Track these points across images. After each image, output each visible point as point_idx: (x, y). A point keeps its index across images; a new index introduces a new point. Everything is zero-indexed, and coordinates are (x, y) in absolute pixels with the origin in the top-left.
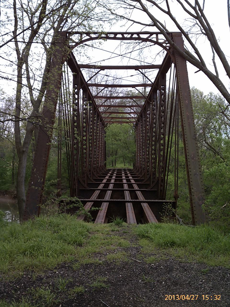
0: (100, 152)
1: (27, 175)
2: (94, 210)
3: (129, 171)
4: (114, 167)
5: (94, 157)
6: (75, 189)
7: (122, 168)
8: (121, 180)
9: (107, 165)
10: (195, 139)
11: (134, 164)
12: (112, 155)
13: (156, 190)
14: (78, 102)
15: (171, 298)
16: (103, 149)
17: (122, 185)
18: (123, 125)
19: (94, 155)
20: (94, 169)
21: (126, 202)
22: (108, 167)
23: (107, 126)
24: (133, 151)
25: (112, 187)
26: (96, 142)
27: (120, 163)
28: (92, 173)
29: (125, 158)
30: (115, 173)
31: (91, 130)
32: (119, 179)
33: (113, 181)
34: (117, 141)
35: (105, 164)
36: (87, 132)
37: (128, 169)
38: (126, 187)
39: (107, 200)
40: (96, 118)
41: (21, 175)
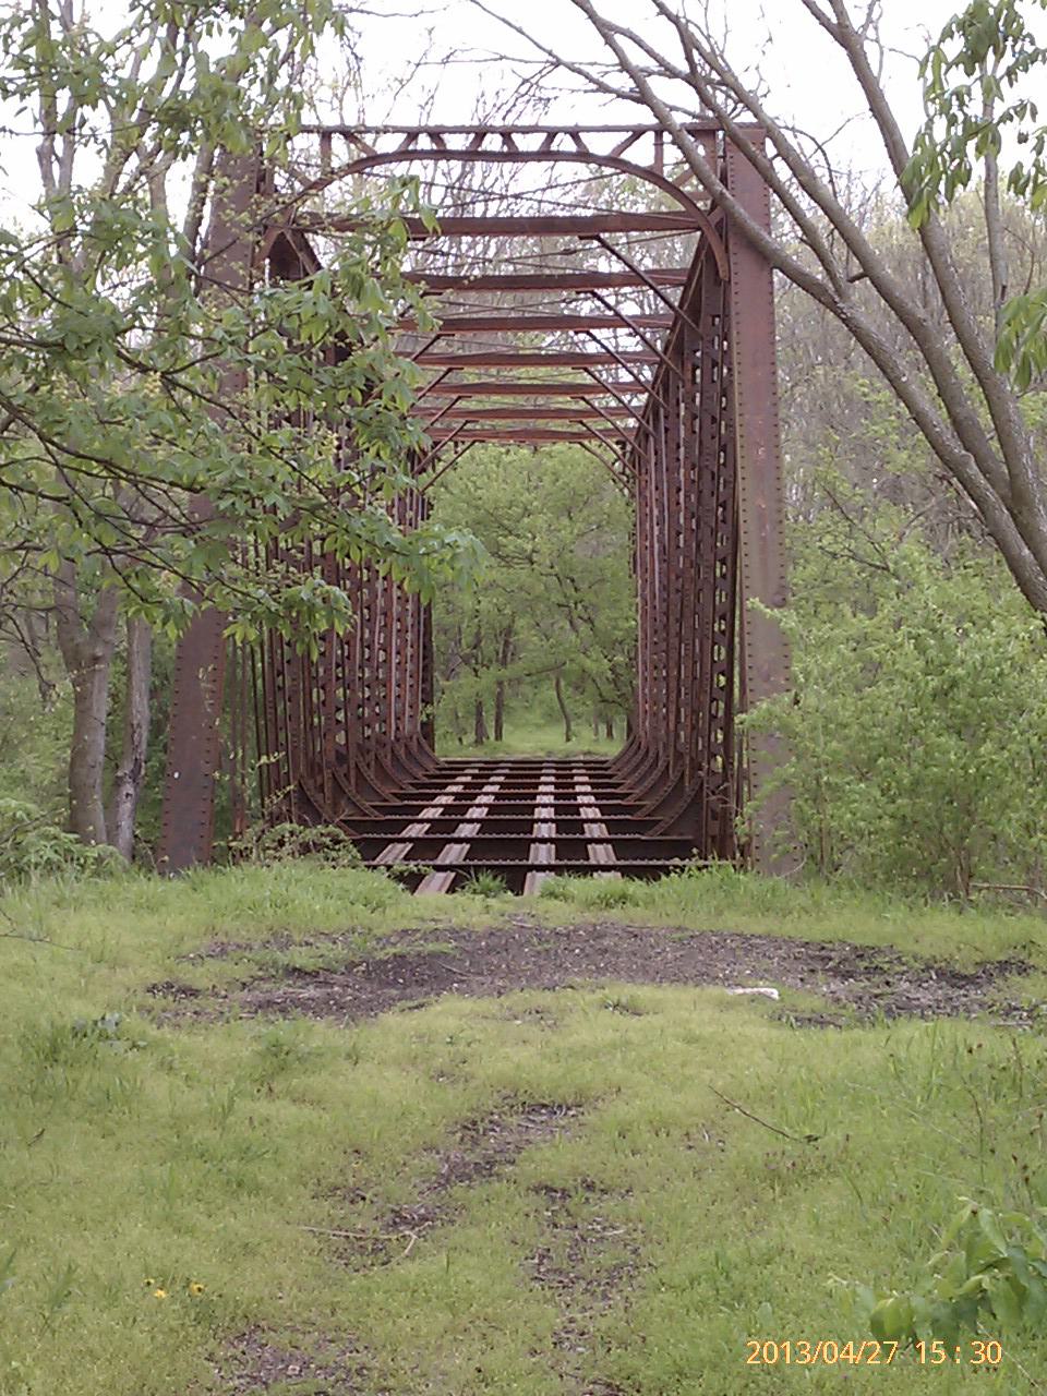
3: (590, 776)
9: (438, 733)
12: (473, 661)
13: (690, 837)
15: (776, 1356)
22: (448, 749)
27: (538, 726)
28: (353, 773)
34: (506, 561)
35: (428, 730)
41: (90, 759)
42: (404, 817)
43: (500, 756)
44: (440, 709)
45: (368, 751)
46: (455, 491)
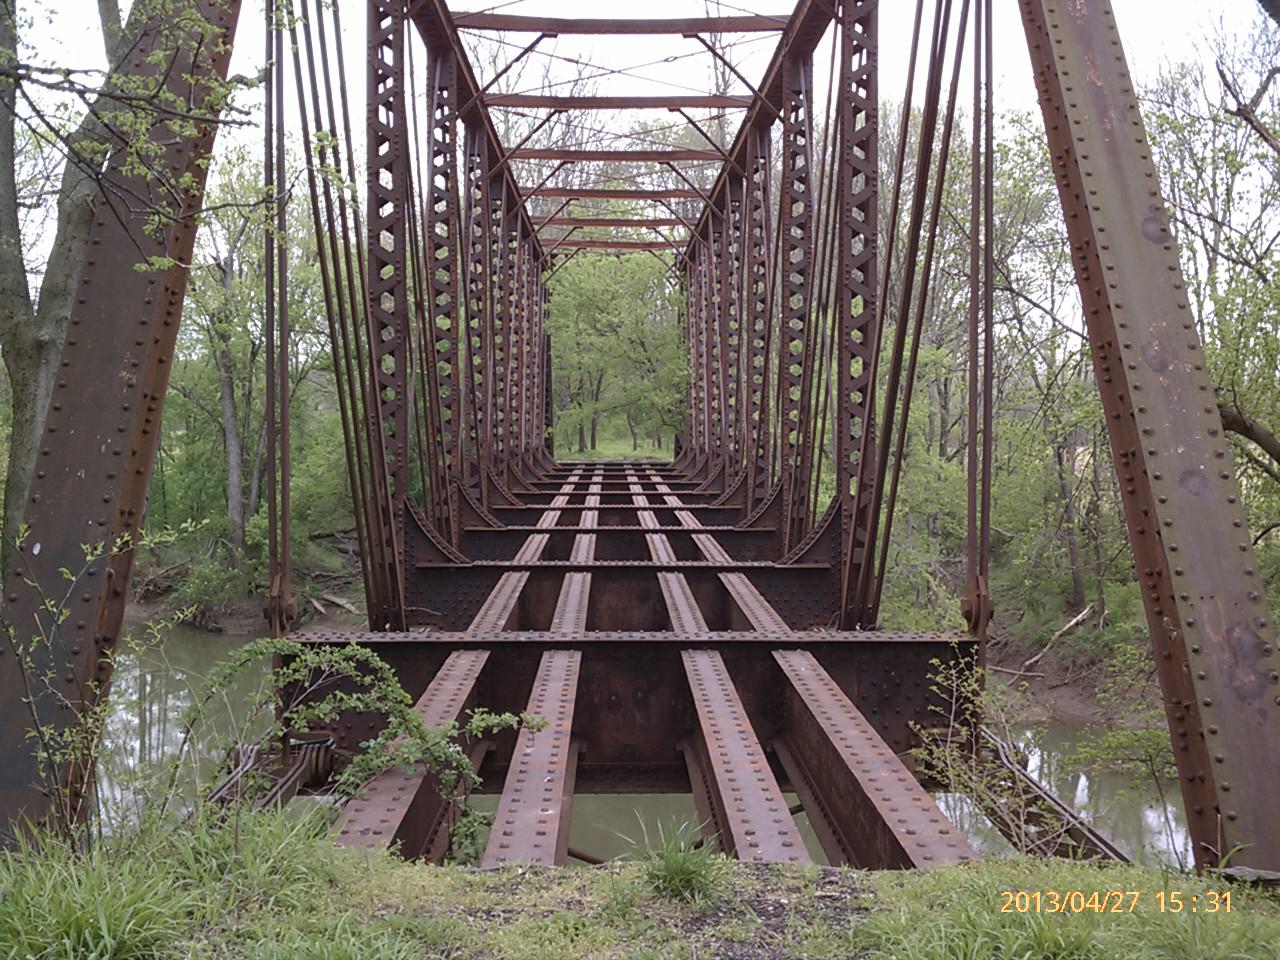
0: (525, 383)
1: (204, 498)
2: (487, 731)
3: (657, 470)
4: (591, 456)
5: (495, 405)
6: (392, 567)
7: (625, 458)
8: (632, 515)
9: (556, 444)
10: (1158, 241)
11: (677, 441)
13: (827, 565)
14: (395, 86)
16: (536, 370)
17: (637, 543)
18: (627, 261)
19: (494, 396)
20: (497, 460)
21: (686, 649)
22: (562, 455)
23: (553, 265)
24: (677, 379)
25: (592, 553)
26: (505, 331)
28: (484, 482)
29: (634, 413)
30: (595, 479)
31: (480, 269)
32: (617, 504)
33: (589, 520)
35: (549, 443)
36: (452, 268)
37: (650, 461)
38: (661, 550)
39: (569, 638)
40: (499, 214)
42: (526, 528)
43: (595, 460)
44: (556, 429)
45: (502, 461)
46: (567, 284)
